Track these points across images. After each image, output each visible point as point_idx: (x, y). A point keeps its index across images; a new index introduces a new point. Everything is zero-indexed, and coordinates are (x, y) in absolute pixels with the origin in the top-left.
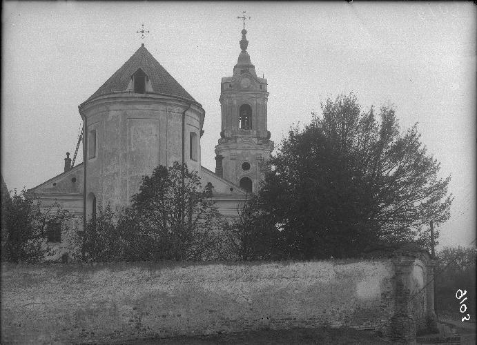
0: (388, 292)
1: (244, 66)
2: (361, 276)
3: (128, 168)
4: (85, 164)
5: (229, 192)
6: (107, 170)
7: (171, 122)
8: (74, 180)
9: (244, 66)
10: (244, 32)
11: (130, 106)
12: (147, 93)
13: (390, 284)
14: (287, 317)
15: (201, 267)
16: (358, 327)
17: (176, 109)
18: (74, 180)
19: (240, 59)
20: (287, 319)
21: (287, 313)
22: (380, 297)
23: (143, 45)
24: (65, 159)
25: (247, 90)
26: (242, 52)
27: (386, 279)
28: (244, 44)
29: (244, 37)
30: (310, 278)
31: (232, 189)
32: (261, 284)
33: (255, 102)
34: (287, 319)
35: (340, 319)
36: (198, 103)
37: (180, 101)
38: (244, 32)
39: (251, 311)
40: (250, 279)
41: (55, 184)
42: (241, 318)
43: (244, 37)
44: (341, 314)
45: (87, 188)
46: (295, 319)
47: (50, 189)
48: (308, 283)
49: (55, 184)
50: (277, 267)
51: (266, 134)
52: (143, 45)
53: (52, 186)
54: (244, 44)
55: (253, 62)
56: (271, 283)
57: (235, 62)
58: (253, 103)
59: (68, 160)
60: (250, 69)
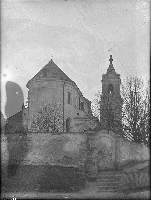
0: (83, 149)
1: (111, 69)
2: (68, 140)
4: (28, 107)
5: (86, 117)
9: (111, 69)
10: (111, 56)
11: (42, 83)
12: (48, 77)
13: (85, 145)
16: (65, 166)
19: (109, 66)
22: (78, 151)
27: (82, 143)
28: (111, 61)
29: (111, 58)
30: (38, 141)
31: (87, 116)
33: (115, 83)
35: (55, 161)
36: (73, 81)
37: (62, 80)
38: (111, 56)
43: (111, 58)
46: (30, 161)
49: (18, 116)
52: (52, 59)
54: (111, 61)
58: (114, 84)
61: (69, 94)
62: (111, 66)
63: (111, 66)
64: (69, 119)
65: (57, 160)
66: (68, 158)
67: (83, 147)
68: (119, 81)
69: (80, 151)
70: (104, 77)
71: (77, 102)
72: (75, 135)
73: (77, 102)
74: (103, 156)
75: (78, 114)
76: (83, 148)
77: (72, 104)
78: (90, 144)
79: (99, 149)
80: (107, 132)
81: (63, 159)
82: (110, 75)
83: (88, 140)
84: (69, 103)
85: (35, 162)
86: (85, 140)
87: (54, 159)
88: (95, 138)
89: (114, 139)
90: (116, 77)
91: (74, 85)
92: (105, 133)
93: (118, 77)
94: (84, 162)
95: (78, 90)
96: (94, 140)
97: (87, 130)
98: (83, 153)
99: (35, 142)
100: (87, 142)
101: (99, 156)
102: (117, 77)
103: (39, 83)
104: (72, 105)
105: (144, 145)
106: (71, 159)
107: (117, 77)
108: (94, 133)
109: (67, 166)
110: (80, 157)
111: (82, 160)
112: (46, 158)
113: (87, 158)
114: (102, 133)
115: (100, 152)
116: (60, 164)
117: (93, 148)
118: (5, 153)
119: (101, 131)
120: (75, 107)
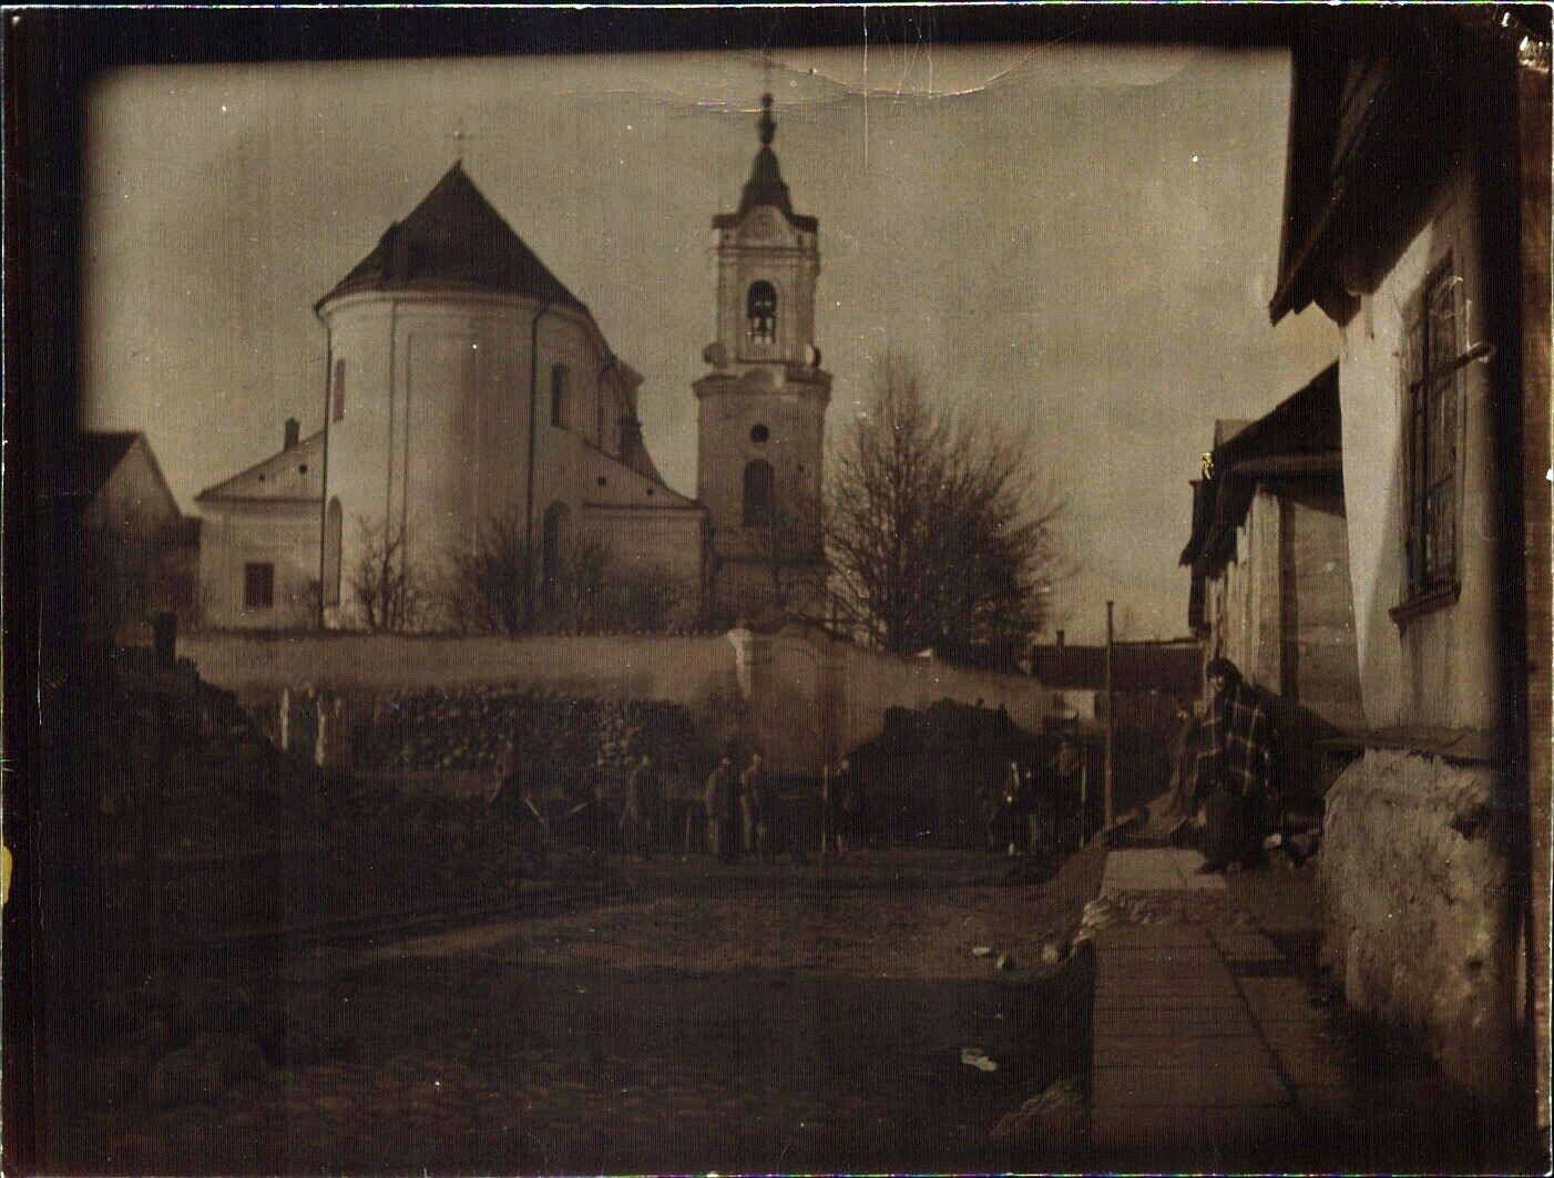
23: (459, 164)
31: (650, 492)
57: (746, 174)
59: (292, 428)
62: (767, 164)
63: (767, 164)
84: (556, 421)
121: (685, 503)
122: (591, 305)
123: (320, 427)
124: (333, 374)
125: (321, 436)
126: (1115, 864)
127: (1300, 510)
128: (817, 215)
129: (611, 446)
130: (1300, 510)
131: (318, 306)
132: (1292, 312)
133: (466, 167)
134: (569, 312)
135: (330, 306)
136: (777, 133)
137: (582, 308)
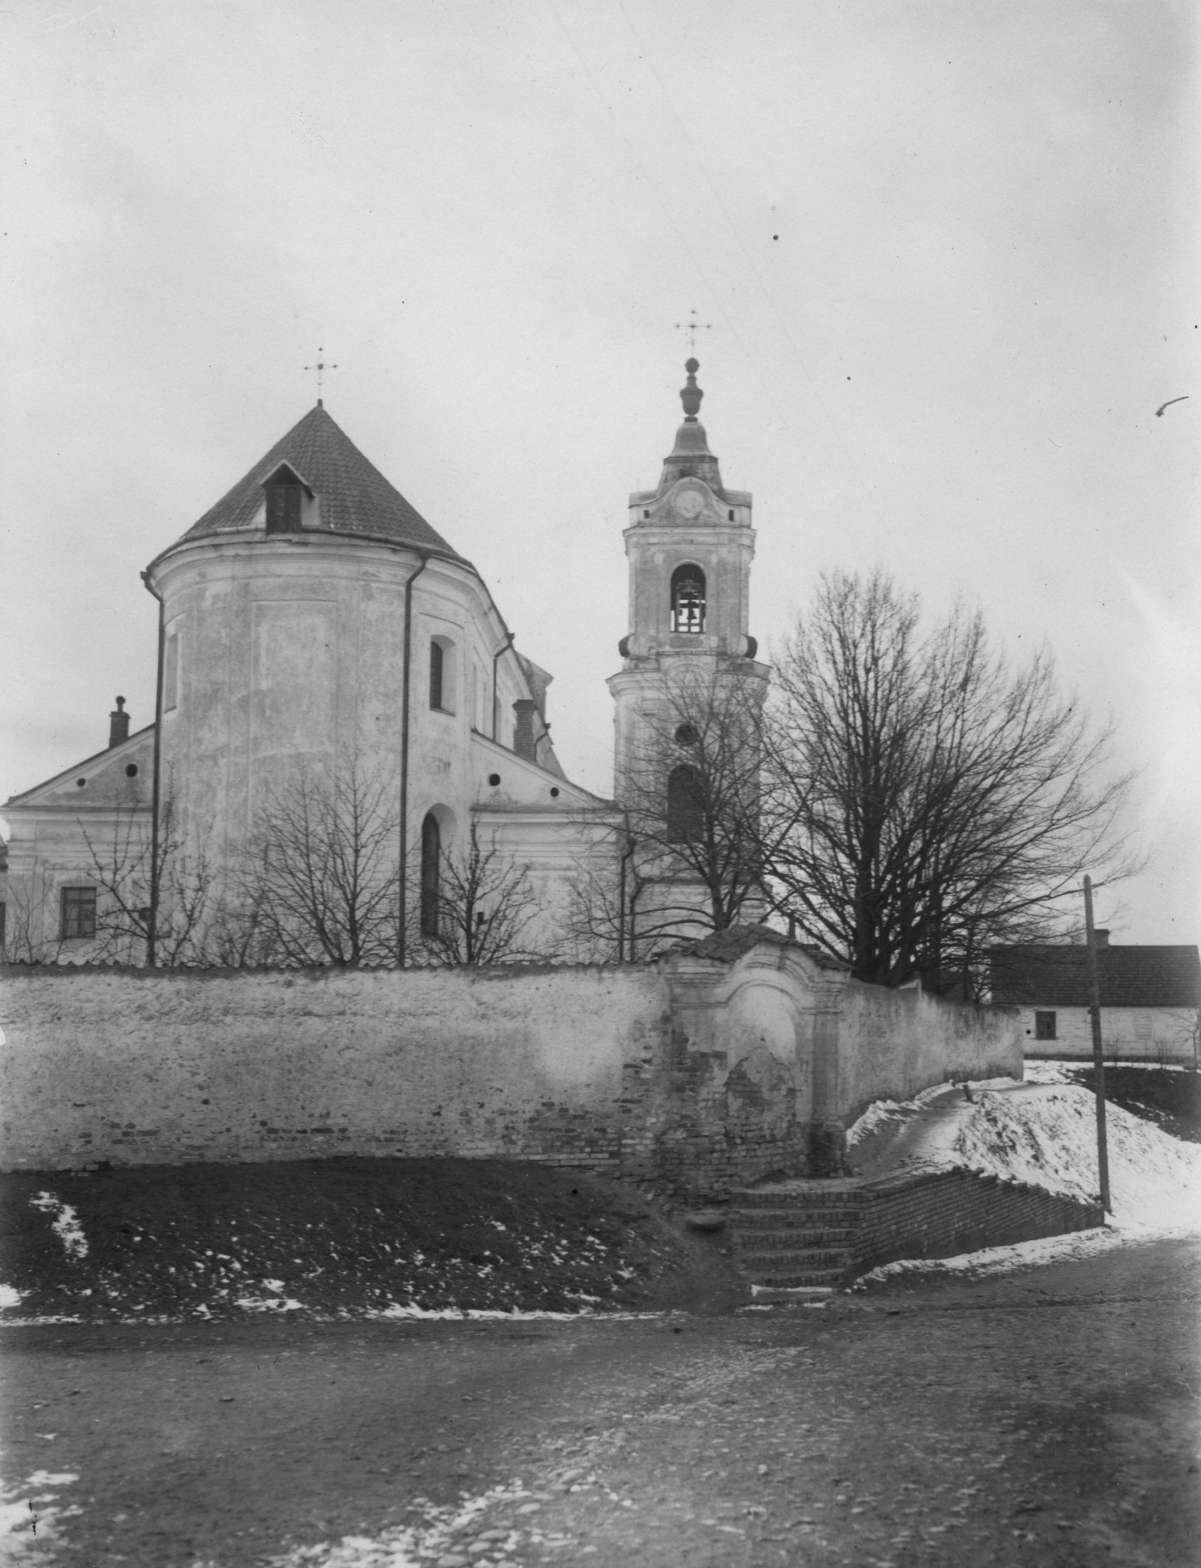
3: (251, 736)
5: (548, 800)
6: (199, 741)
7: (372, 609)
8: (132, 771)
10: (692, 366)
11: (260, 567)
13: (654, 1039)
14: (316, 1125)
15: (51, 980)
17: (386, 574)
18: (132, 771)
20: (318, 1131)
21: (317, 1113)
22: (618, 1073)
23: (320, 402)
24: (113, 714)
25: (696, 521)
26: (687, 420)
28: (692, 398)
29: (692, 379)
31: (555, 792)
32: (238, 1029)
34: (318, 1131)
35: (490, 1135)
38: (692, 366)
39: (204, 1107)
40: (203, 1016)
41: (81, 782)
42: (172, 1125)
43: (692, 379)
44: (490, 1122)
45: (161, 792)
46: (343, 1130)
47: (68, 796)
48: (385, 1032)
49: (81, 782)
50: (289, 984)
51: (744, 647)
52: (320, 402)
53: (73, 787)
54: (692, 398)
55: (714, 446)
56: (265, 1028)
57: (668, 447)
58: (710, 562)
59: (120, 720)
60: (706, 466)
61: (438, 651)
62: (692, 436)
63: (692, 436)
64: (437, 816)
65: (500, 1123)
66: (564, 1111)
67: (647, 1048)
68: (746, 541)
69: (630, 1071)
70: (647, 514)
71: (480, 692)
72: (600, 980)
73: (480, 692)
74: (752, 1097)
75: (495, 780)
76: (645, 1055)
77: (461, 711)
78: (689, 1031)
79: (732, 1060)
80: (772, 959)
81: (532, 1120)
82: (689, 500)
83: (674, 1013)
84: (436, 703)
85: (378, 1140)
86: (660, 1013)
87: (481, 1121)
88: (712, 1000)
89: (809, 1000)
90: (724, 510)
91: (473, 583)
92: (764, 965)
93: (736, 516)
94: (650, 1135)
95: (492, 616)
96: (710, 1012)
97: (674, 952)
98: (644, 1082)
99: (373, 1022)
100: (666, 1019)
101: (731, 1100)
102: (731, 515)
103: (241, 570)
104: (459, 726)
105: (920, 991)
106: (575, 1117)
107: (731, 515)
108: (711, 970)
109: (556, 1156)
110: (630, 1106)
111: (639, 1123)
112: (438, 1114)
113: (667, 1112)
114: (750, 967)
115: (737, 1080)
116: (518, 1149)
117: (704, 1055)
118: (201, 1088)
119: (748, 957)
120: (474, 731)
121: (596, 805)
122: (475, 564)
123: (152, 720)
124: (1129, 1064)
125: (152, 732)
126: (1072, 1312)
127: (1104, 1013)
128: (749, 490)
129: (507, 737)
130: (1104, 1013)
131: (147, 576)
132: (1113, 941)
133: (326, 407)
134: (459, 575)
135: (161, 572)
136: (704, 403)
137: (466, 566)
